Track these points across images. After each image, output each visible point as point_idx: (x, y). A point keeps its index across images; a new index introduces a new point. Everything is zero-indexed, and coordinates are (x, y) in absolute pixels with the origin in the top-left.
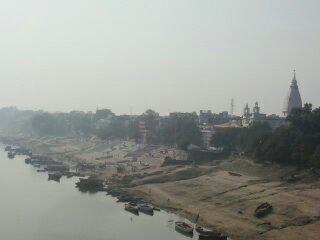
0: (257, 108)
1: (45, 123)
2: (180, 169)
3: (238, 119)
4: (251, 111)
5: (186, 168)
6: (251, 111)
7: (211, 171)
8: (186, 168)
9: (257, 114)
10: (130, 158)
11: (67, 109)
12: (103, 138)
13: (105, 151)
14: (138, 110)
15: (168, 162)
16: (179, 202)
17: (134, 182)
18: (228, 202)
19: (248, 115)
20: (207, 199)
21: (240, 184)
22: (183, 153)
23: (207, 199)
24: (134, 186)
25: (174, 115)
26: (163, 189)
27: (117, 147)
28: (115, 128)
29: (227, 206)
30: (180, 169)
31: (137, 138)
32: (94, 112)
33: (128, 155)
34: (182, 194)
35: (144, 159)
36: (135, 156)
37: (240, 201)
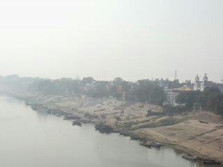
0: (206, 78)
1: (46, 86)
2: (161, 119)
3: (188, 84)
4: (201, 80)
5: (165, 118)
6: (201, 80)
7: (148, 126)
8: (165, 118)
9: (206, 82)
10: (119, 111)
11: (59, 77)
12: (93, 97)
13: (97, 105)
14: (110, 78)
15: (150, 113)
16: (174, 140)
17: (133, 126)
18: (208, 141)
19: (198, 83)
20: (193, 138)
21: (211, 129)
22: (159, 107)
23: (193, 138)
24: (134, 129)
25: (141, 82)
26: (158, 132)
27: (105, 103)
28: (120, 90)
29: (209, 143)
30: (161, 119)
31: (118, 97)
32: (82, 79)
33: (115, 109)
34: (173, 135)
35: (127, 111)
36: (122, 108)
37: (217, 140)
